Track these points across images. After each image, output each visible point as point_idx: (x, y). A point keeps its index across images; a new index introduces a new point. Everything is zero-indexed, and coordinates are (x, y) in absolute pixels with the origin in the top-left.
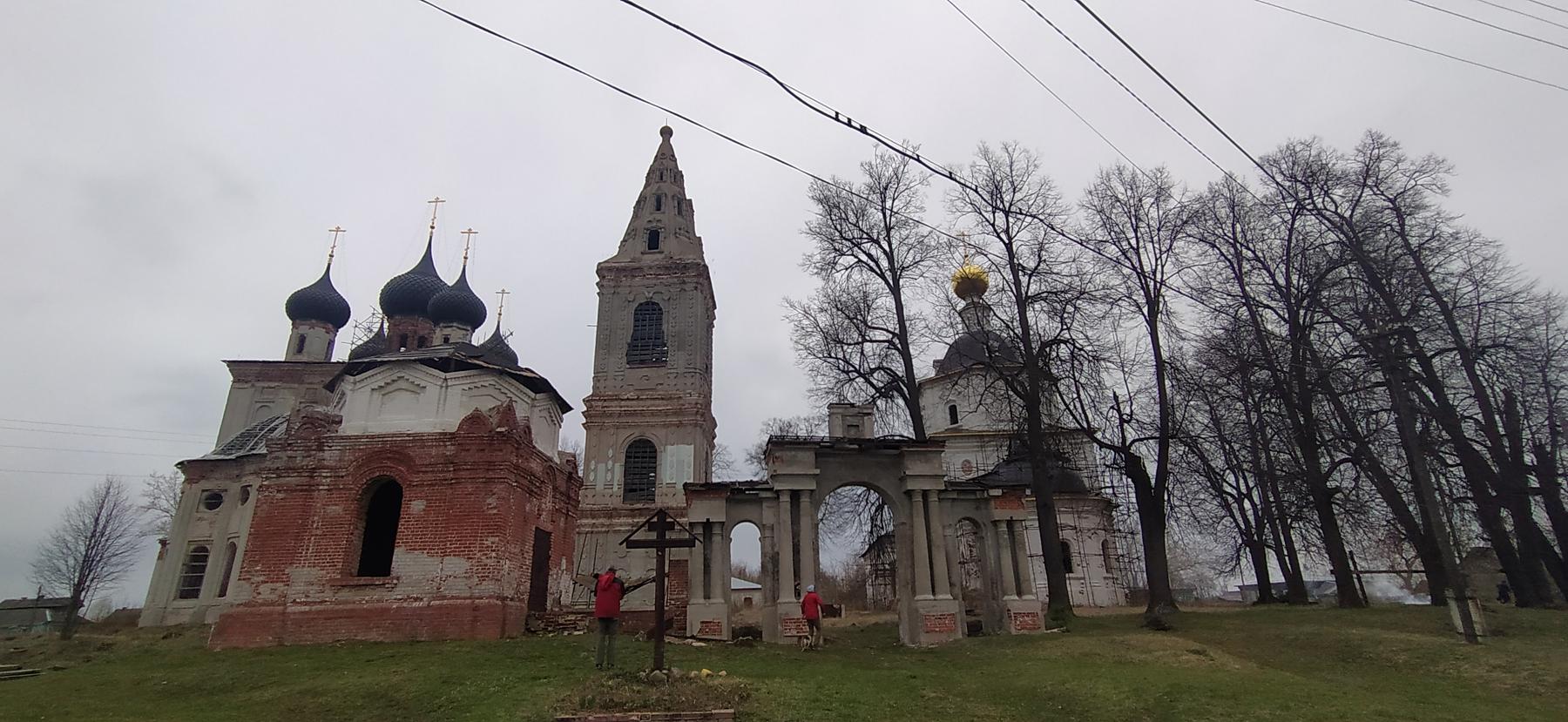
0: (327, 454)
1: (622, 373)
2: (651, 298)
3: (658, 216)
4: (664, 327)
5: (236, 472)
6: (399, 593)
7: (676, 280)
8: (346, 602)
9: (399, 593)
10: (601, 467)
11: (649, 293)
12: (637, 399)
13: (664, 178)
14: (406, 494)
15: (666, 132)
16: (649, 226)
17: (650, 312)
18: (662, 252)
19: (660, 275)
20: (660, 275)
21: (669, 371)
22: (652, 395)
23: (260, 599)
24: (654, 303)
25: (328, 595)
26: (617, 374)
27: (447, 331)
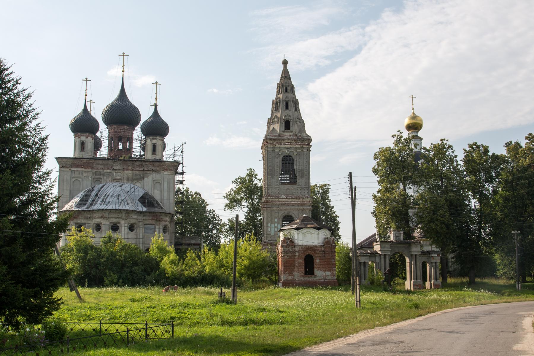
0: (296, 249)
1: (278, 187)
2: (289, 154)
3: (287, 112)
4: (295, 167)
5: (89, 216)
6: (317, 279)
7: (299, 146)
8: (306, 280)
9: (317, 279)
10: (273, 226)
11: (288, 151)
12: (286, 198)
13: (288, 91)
14: (314, 258)
15: (285, 63)
16: (286, 118)
17: (289, 160)
18: (292, 132)
19: (292, 143)
20: (292, 143)
21: (298, 187)
22: (292, 197)
23: (289, 279)
24: (290, 156)
25: (302, 278)
26: (276, 187)
27: (154, 141)
